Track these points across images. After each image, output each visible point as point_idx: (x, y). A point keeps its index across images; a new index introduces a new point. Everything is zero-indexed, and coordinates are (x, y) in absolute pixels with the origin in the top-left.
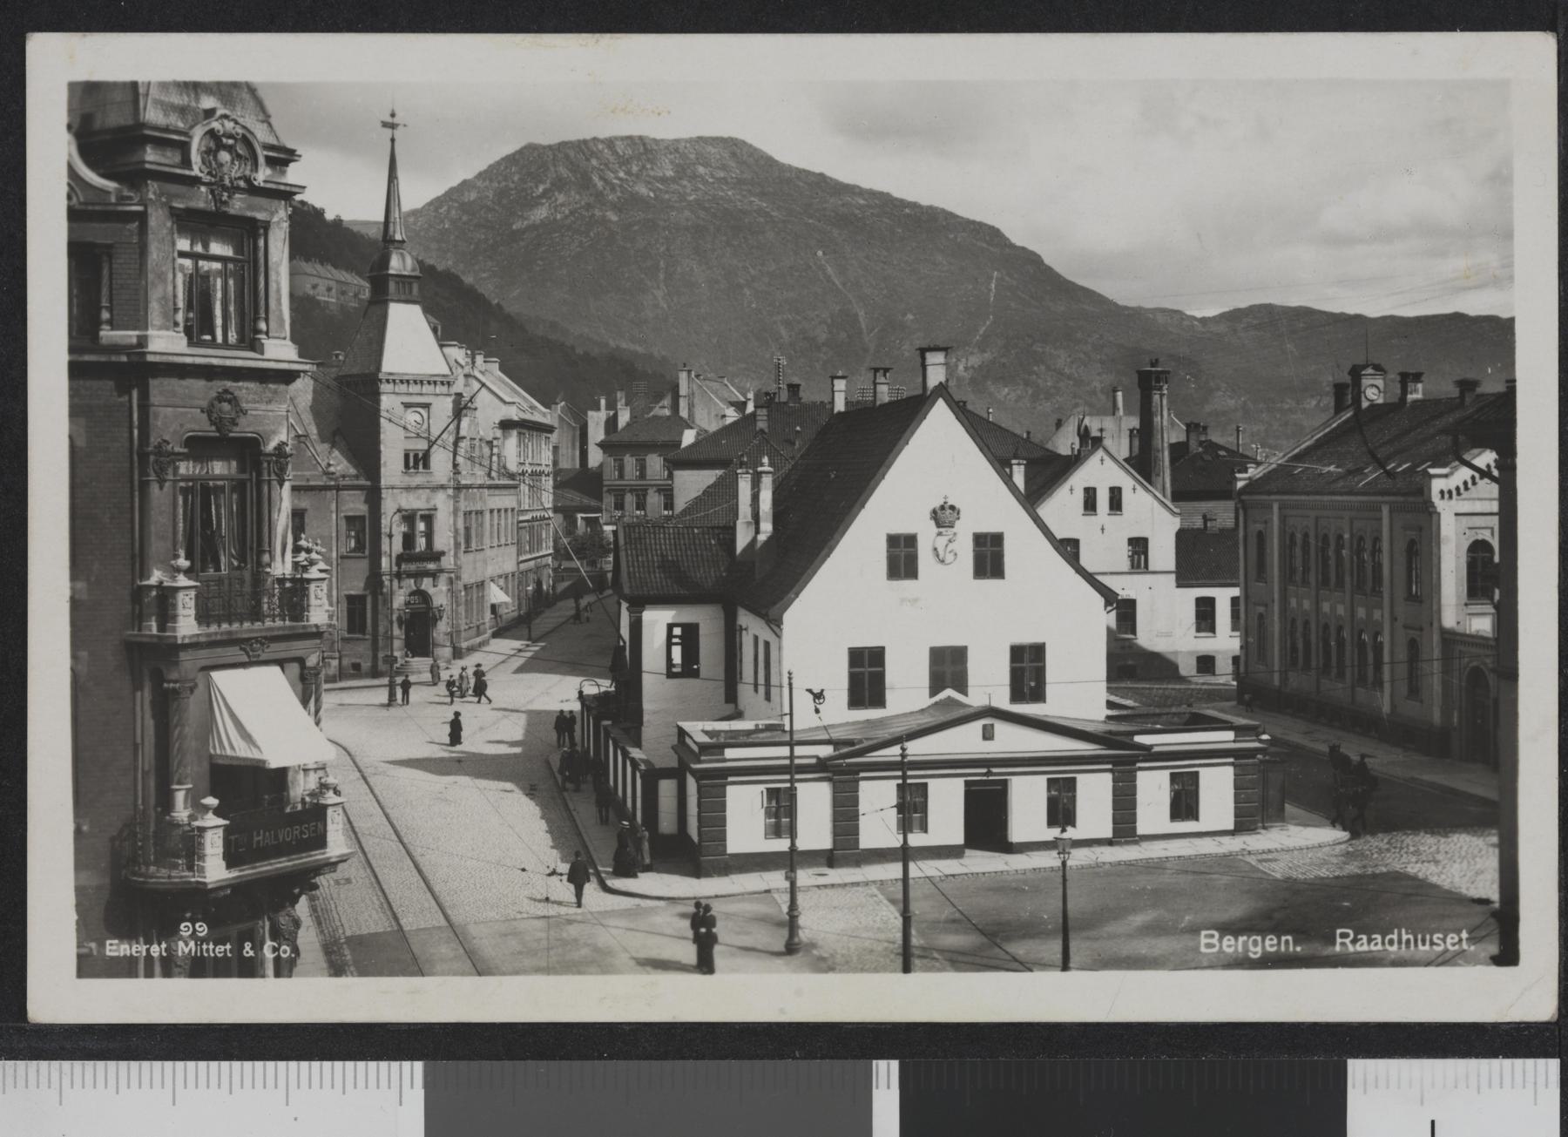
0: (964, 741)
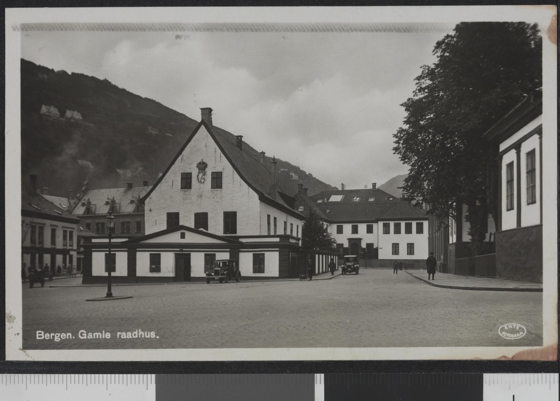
0: (174, 238)
